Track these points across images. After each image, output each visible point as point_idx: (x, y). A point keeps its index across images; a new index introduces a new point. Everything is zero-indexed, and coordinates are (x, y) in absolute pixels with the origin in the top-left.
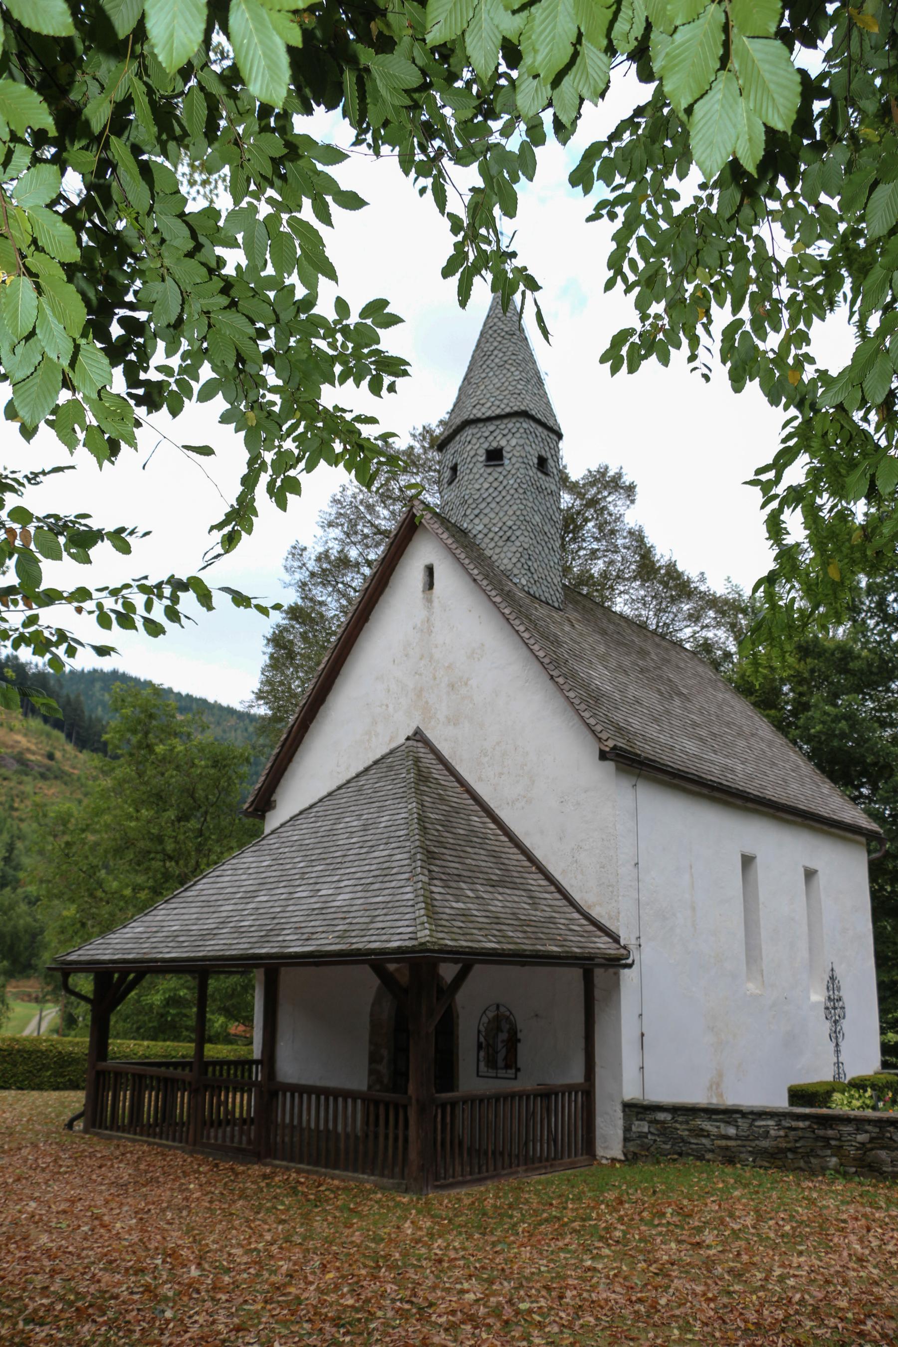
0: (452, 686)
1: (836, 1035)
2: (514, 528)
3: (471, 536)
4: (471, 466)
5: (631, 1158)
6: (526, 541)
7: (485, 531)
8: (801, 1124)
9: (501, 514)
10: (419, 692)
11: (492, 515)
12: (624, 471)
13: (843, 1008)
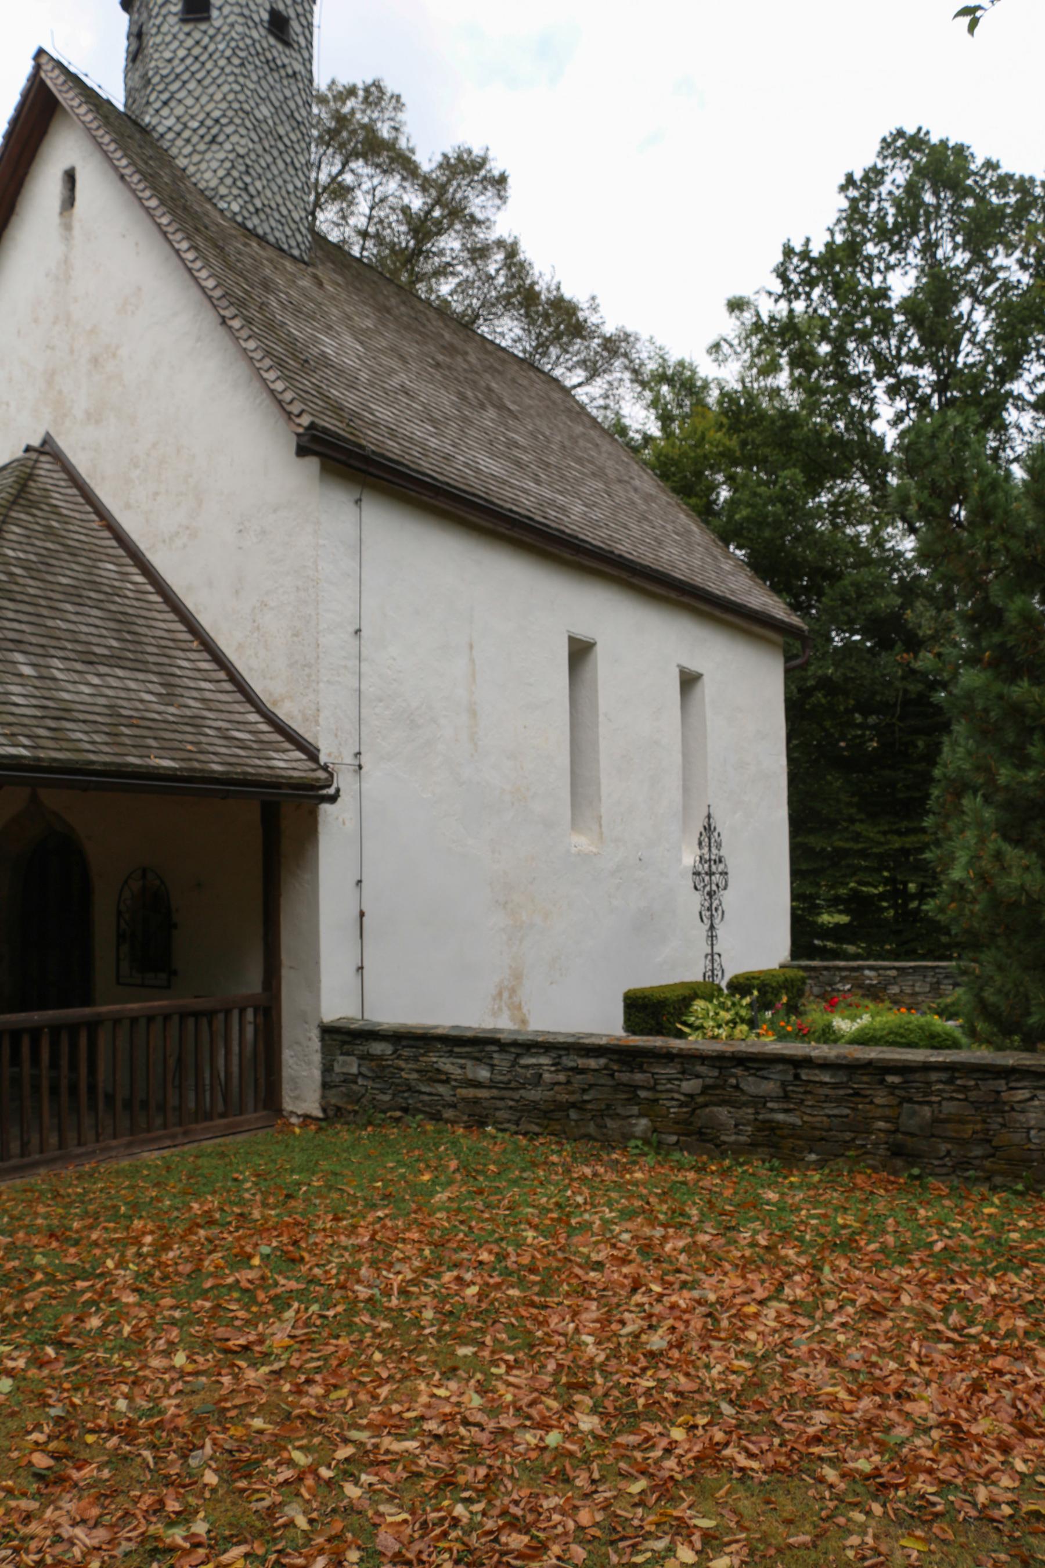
0: (95, 361)
1: (711, 913)
2: (223, 121)
3: (156, 135)
4: (158, 21)
5: (332, 1114)
6: (243, 145)
7: (178, 127)
8: (593, 1063)
9: (204, 100)
10: (51, 377)
11: (190, 101)
12: (491, 155)
13: (724, 873)
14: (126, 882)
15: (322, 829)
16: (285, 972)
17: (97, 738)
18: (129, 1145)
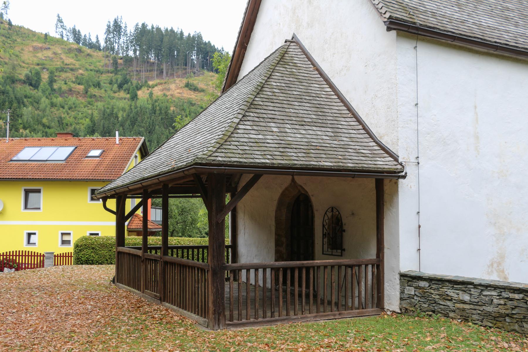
5: (404, 311)
8: (516, 296)
14: (326, 213)
15: (400, 189)
16: (386, 250)
17: (300, 155)
18: (316, 317)
